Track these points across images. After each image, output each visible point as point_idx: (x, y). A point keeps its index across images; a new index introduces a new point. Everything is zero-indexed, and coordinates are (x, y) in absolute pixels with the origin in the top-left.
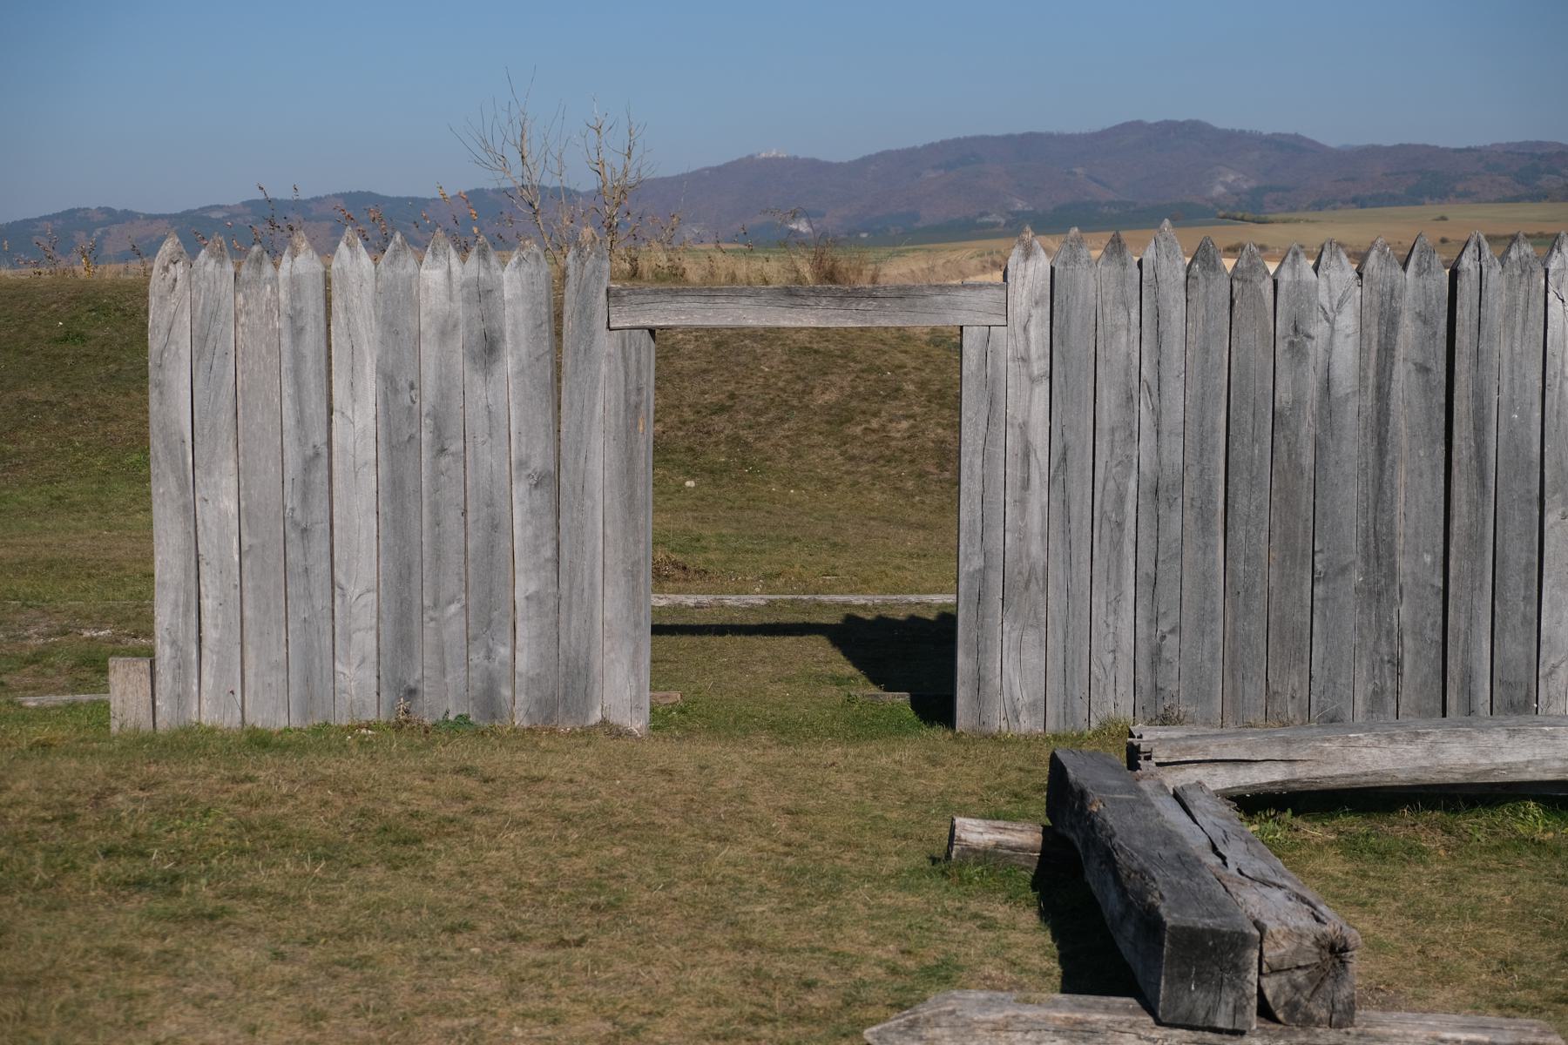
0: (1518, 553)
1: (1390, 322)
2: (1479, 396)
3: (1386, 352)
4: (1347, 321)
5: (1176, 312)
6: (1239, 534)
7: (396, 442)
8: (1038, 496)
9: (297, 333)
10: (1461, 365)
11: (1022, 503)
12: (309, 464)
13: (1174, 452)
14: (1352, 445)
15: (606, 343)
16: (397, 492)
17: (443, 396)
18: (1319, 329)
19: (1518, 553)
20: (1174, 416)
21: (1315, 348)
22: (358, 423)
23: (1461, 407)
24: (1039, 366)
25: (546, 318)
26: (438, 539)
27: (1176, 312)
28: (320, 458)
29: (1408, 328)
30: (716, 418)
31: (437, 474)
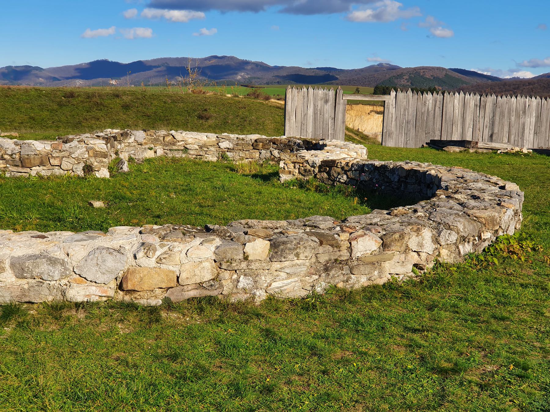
0: (450, 131)
1: (436, 102)
2: (446, 111)
3: (435, 105)
4: (431, 101)
5: (411, 100)
6: (417, 128)
7: (315, 114)
8: (393, 123)
9: (304, 99)
10: (444, 108)
11: (391, 123)
12: (305, 115)
13: (410, 118)
14: (431, 116)
15: (342, 101)
16: (315, 119)
17: (321, 107)
18: (428, 102)
19: (450, 131)
20: (410, 113)
21: (427, 105)
22: (311, 111)
23: (444, 113)
24: (394, 106)
25: (375, 282)
26: (319, 126)
27: (411, 100)
28: (306, 115)
29: (438, 102)
30: (500, 330)
31: (320, 117)
